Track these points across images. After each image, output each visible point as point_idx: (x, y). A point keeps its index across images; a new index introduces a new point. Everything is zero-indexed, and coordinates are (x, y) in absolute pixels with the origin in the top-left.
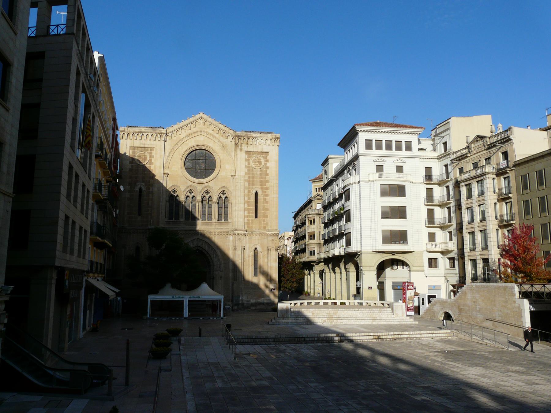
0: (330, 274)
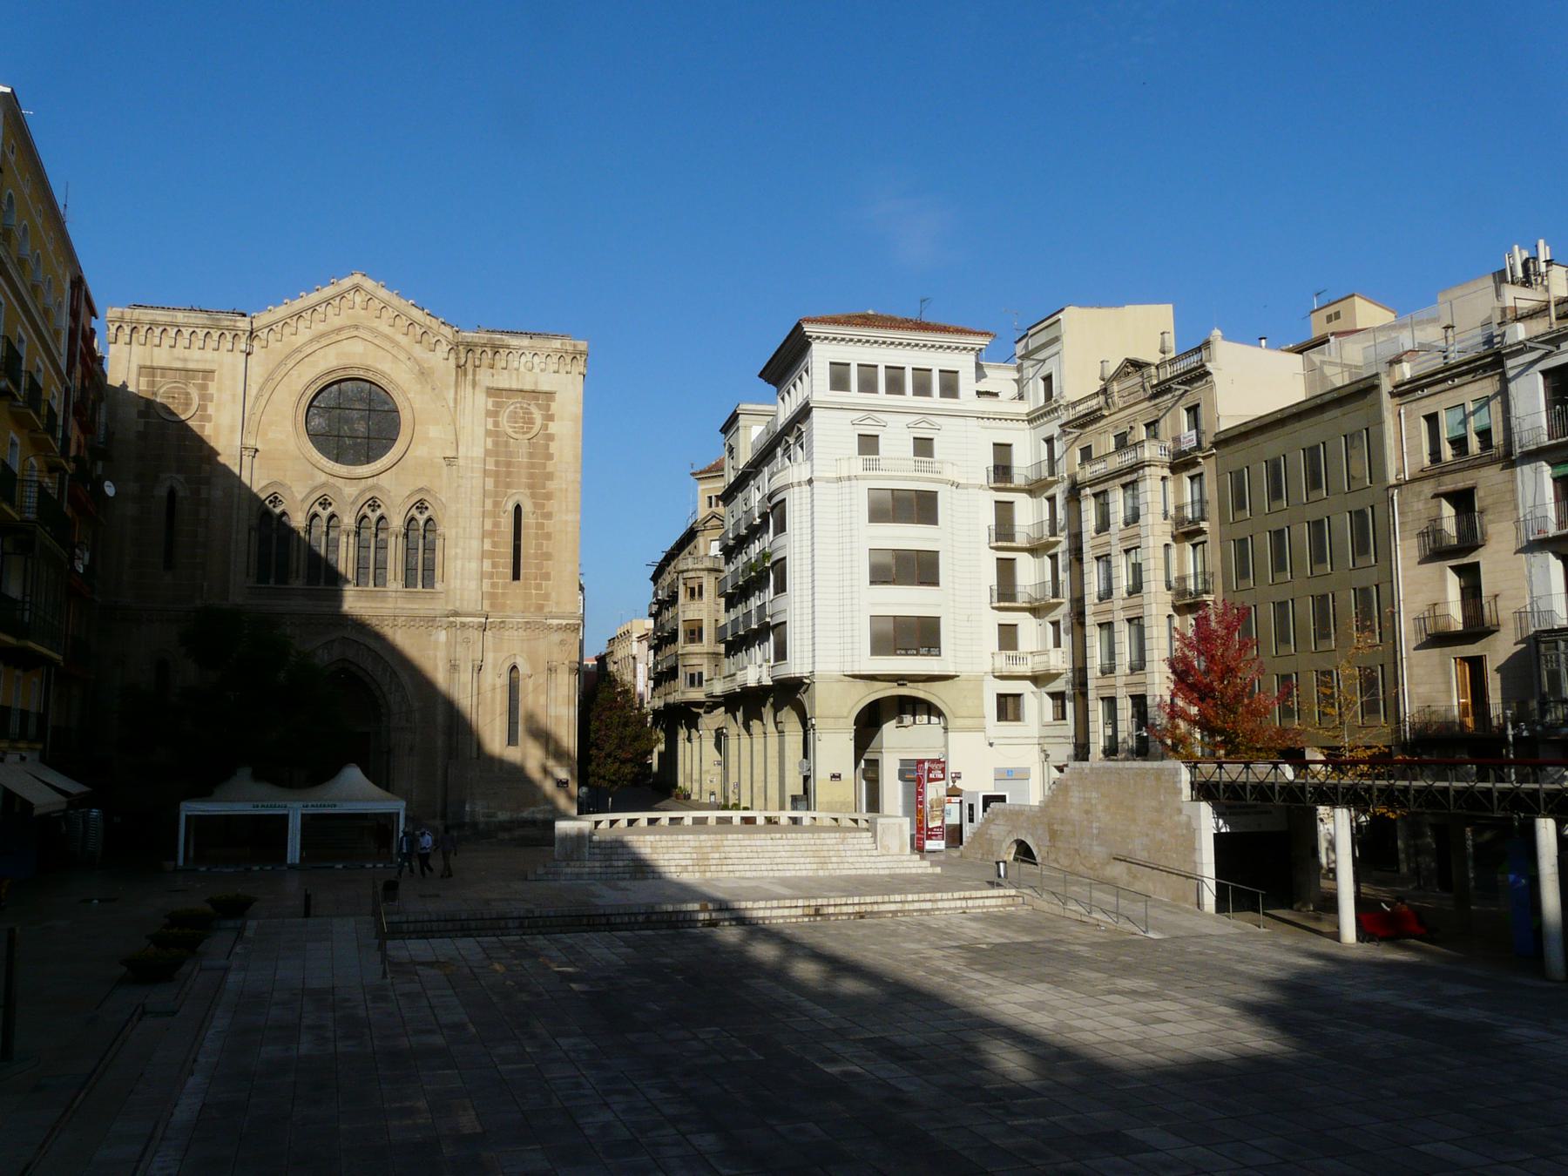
0: (765, 737)
